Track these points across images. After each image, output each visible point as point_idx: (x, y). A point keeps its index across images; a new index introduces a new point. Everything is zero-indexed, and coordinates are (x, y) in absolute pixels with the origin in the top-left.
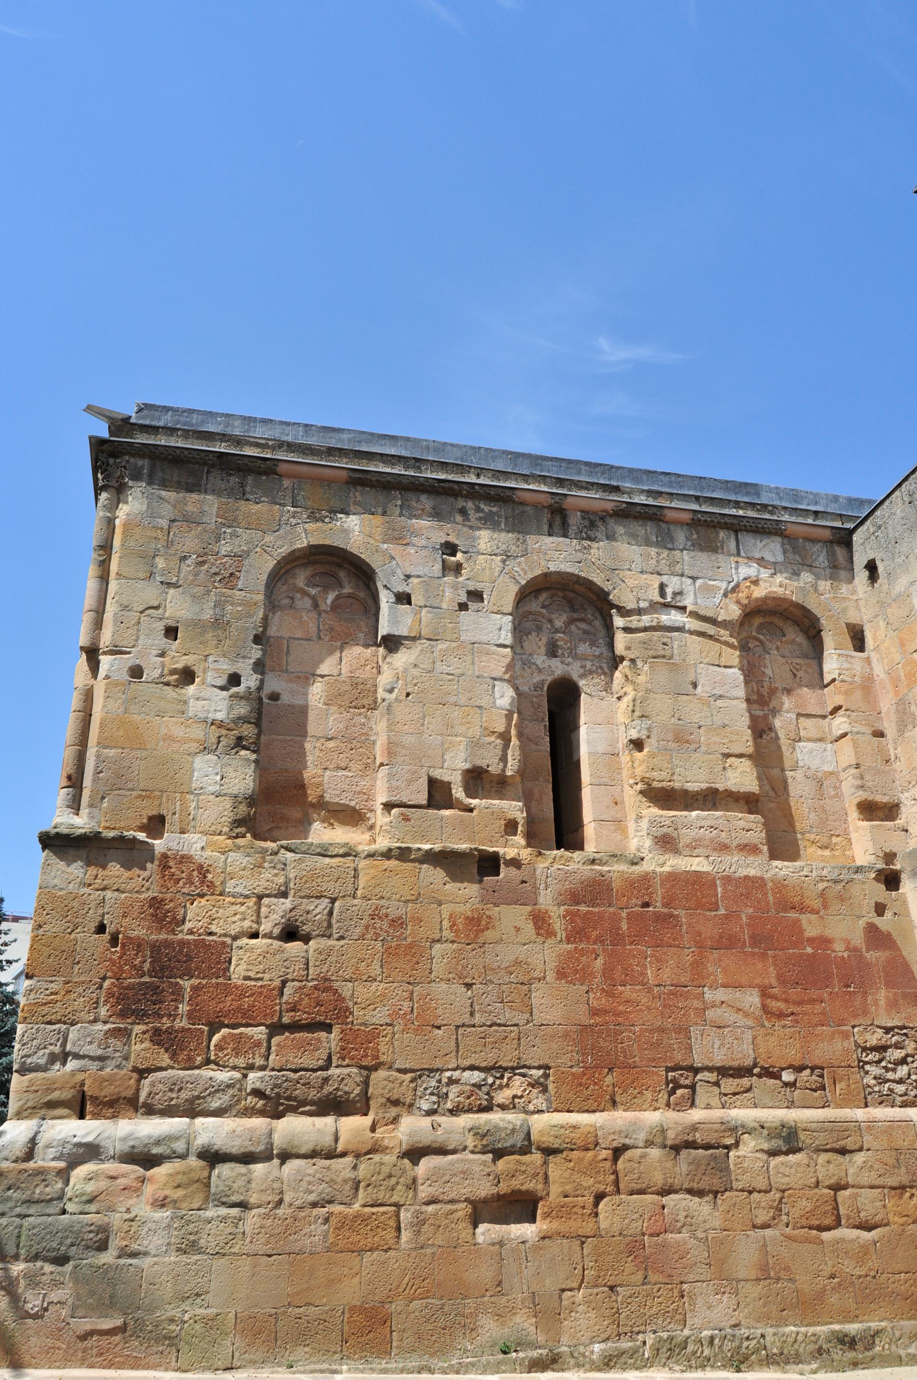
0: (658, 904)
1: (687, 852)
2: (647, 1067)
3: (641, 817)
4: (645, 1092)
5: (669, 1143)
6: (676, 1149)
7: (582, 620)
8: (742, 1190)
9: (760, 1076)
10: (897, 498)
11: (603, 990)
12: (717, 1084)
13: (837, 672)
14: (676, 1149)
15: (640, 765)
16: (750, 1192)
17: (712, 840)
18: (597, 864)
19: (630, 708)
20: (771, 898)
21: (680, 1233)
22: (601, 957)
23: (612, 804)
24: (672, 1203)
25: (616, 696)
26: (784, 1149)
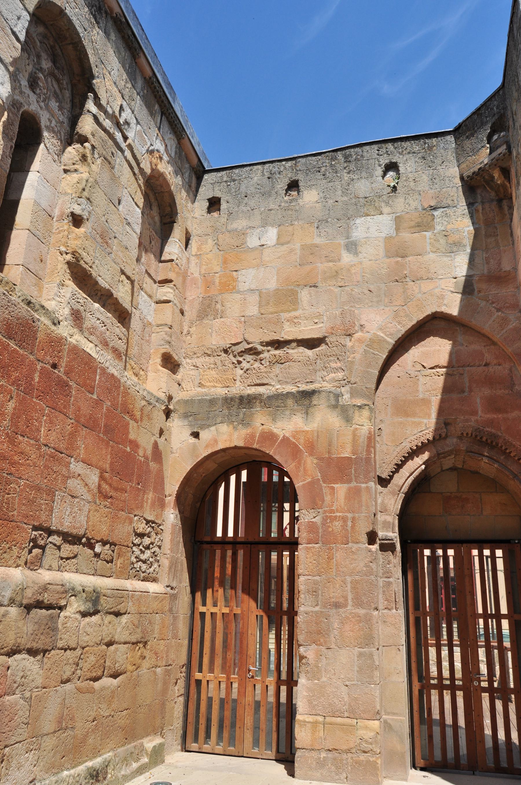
0: (62, 369)
1: (86, 334)
2: (21, 522)
3: (63, 285)
4: (13, 547)
5: (25, 602)
6: (28, 608)
7: (58, 81)
8: (62, 649)
9: (84, 545)
10: (258, 169)
11: (7, 434)
12: (59, 548)
13: (176, 256)
14: (28, 608)
15: (75, 239)
16: (66, 650)
17: (102, 333)
18: (30, 307)
19: (81, 187)
20: (120, 399)
21: (14, 694)
22: (13, 401)
23: (39, 260)
24: (15, 664)
25: (63, 167)
26: (91, 611)
